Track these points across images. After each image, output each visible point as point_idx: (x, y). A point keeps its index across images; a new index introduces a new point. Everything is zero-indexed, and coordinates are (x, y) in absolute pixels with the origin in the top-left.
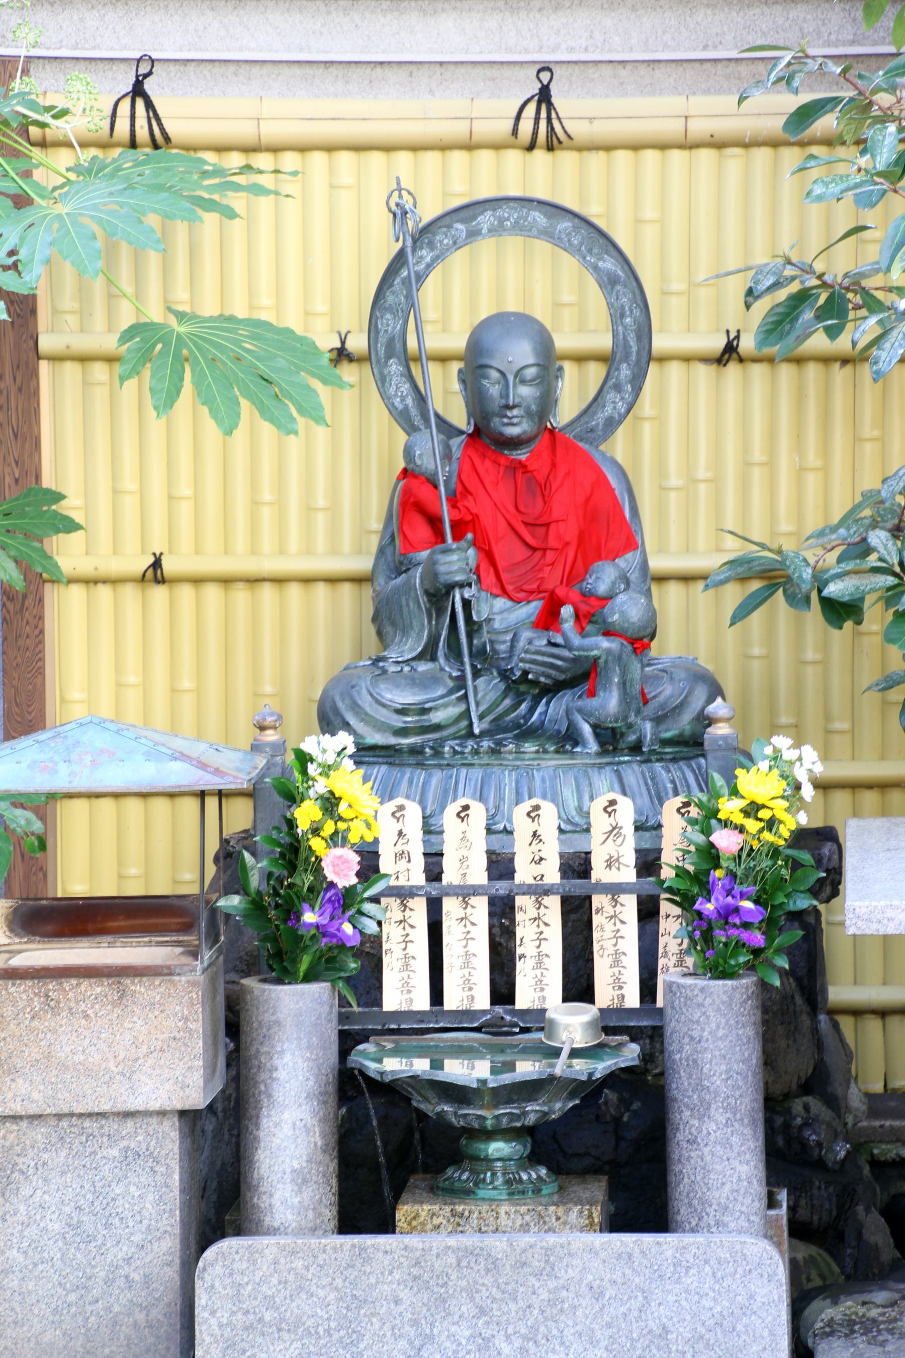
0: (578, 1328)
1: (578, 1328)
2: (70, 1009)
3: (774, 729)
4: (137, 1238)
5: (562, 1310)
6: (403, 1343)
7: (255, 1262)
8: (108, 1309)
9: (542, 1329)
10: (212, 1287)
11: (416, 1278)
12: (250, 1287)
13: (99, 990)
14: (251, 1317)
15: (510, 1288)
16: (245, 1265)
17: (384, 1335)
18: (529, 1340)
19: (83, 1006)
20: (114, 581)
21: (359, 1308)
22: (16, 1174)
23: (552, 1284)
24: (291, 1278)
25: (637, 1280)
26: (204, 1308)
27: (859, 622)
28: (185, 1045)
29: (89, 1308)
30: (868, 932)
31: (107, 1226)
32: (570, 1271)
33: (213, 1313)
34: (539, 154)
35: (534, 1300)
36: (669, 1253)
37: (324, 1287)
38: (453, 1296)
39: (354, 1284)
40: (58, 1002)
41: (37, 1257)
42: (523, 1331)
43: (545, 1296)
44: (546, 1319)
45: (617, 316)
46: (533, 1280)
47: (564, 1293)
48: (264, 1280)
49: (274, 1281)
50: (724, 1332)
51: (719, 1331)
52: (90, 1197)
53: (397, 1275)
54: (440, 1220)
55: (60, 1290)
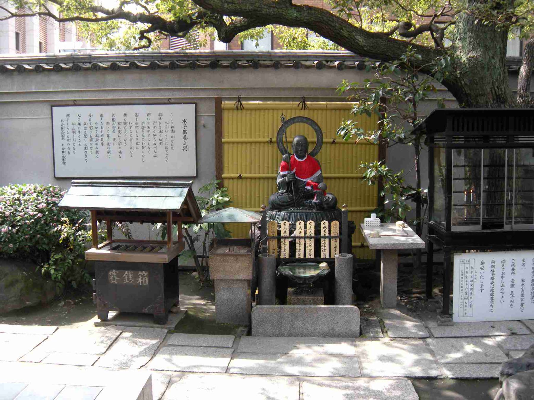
3: (56, 281)
20: (233, 178)
27: (230, 232)
34: (303, 111)
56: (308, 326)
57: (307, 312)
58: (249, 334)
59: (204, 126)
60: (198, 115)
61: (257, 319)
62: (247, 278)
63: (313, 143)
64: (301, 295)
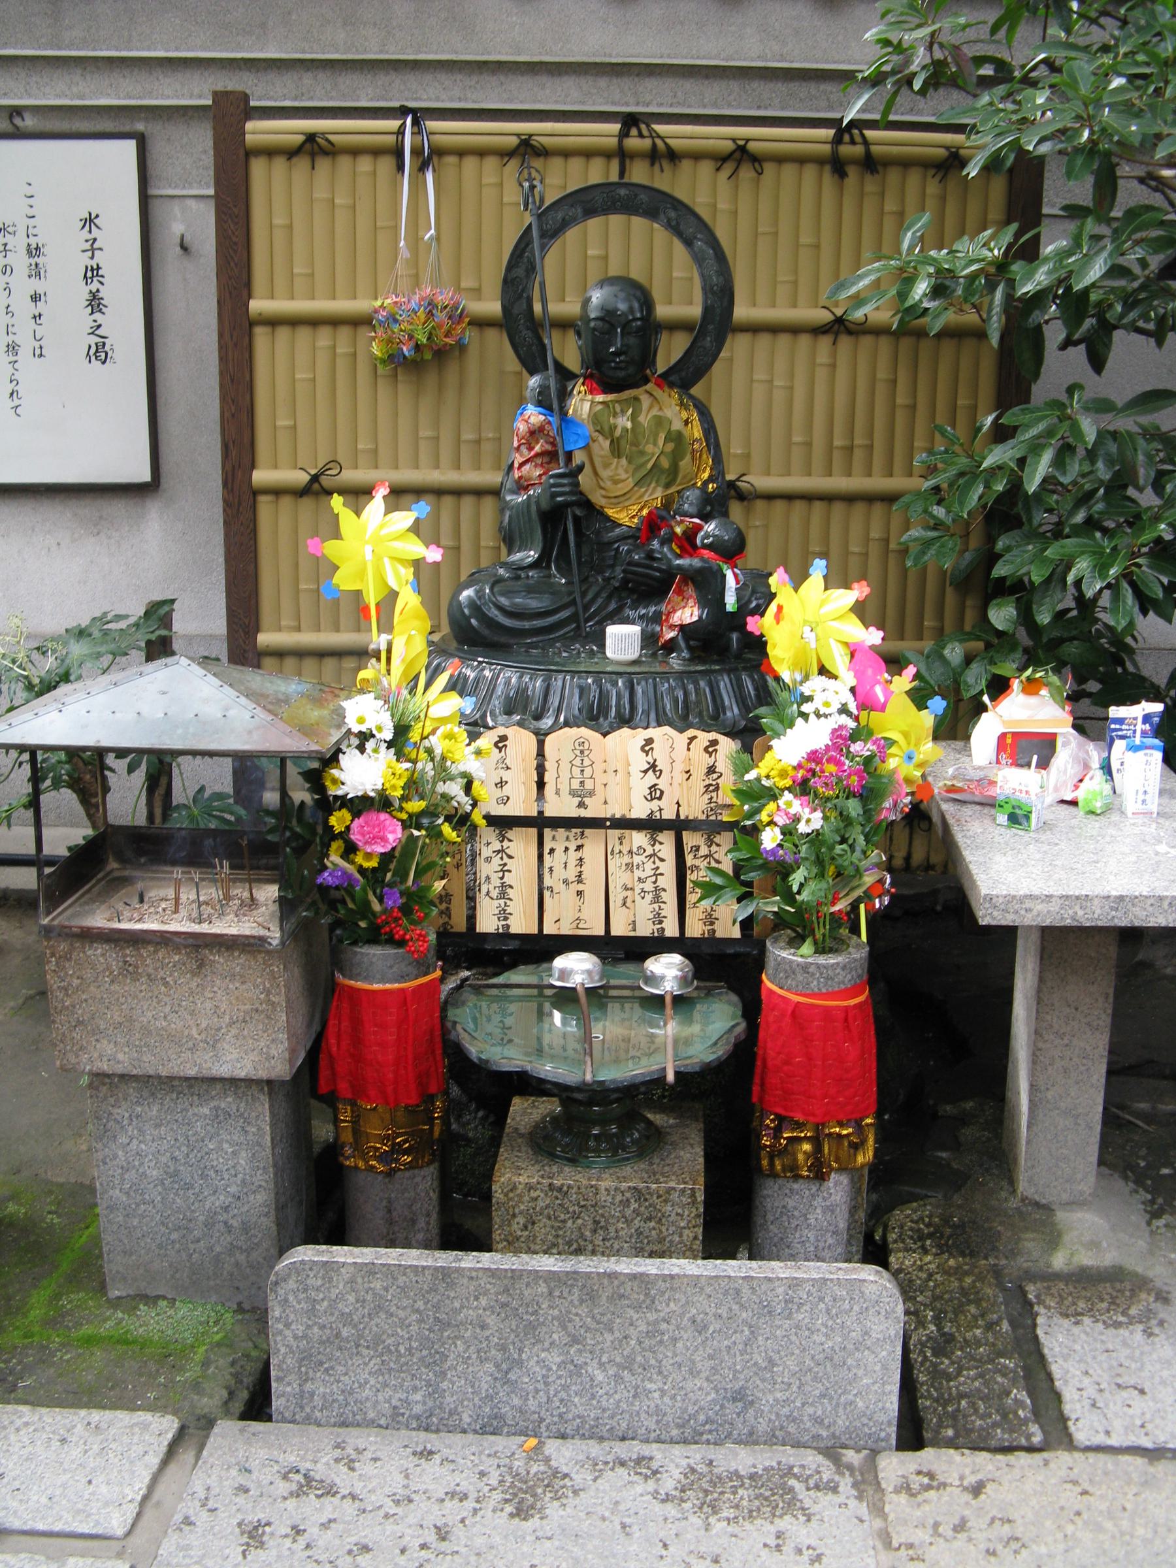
0: (678, 1359)
1: (678, 1359)
2: (149, 975)
4: (233, 1189)
5: (661, 1342)
6: (489, 1367)
7: (331, 1280)
8: (211, 1249)
9: (639, 1359)
10: (286, 1300)
11: (504, 1305)
12: (325, 1303)
13: (177, 958)
14: (328, 1332)
15: (605, 1319)
16: (320, 1282)
17: (469, 1358)
18: (624, 1368)
19: (161, 974)
21: (442, 1330)
22: (111, 1123)
23: (652, 1317)
24: (369, 1297)
25: (744, 1315)
26: (278, 1320)
28: (268, 1017)
29: (192, 1246)
30: (1004, 923)
31: (203, 1176)
32: (672, 1304)
33: (287, 1325)
35: (632, 1331)
36: (780, 1290)
37: (404, 1308)
38: (543, 1324)
39: (437, 1307)
40: (137, 967)
41: (139, 1198)
42: (618, 1360)
43: (643, 1328)
44: (644, 1350)
45: (707, 290)
46: (631, 1312)
47: (664, 1326)
48: (340, 1297)
49: (351, 1298)
50: (835, 1367)
51: (828, 1365)
52: (184, 1149)
53: (483, 1302)
54: (538, 1193)
55: (163, 1229)
56: (600, 1376)
57: (590, 1296)
58: (257, 1406)
59: (184, 248)
60: (152, 191)
61: (299, 1329)
62: (263, 1074)
63: (675, 326)
64: (573, 1161)
